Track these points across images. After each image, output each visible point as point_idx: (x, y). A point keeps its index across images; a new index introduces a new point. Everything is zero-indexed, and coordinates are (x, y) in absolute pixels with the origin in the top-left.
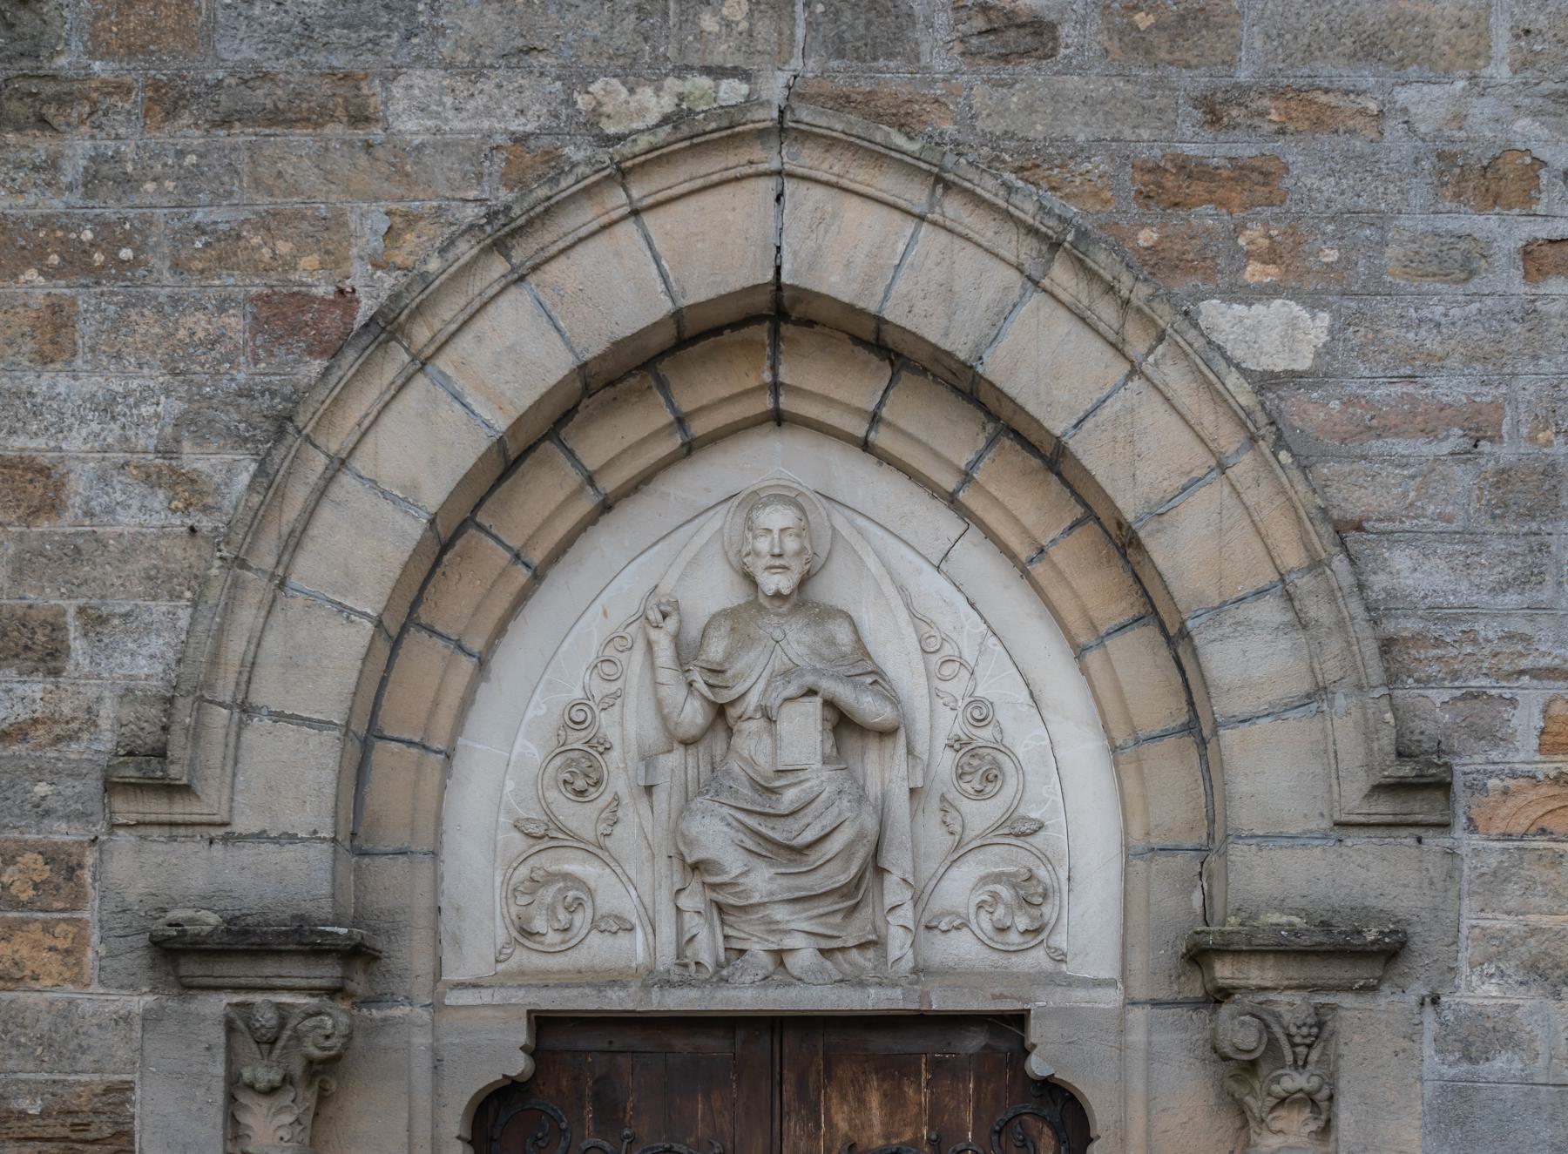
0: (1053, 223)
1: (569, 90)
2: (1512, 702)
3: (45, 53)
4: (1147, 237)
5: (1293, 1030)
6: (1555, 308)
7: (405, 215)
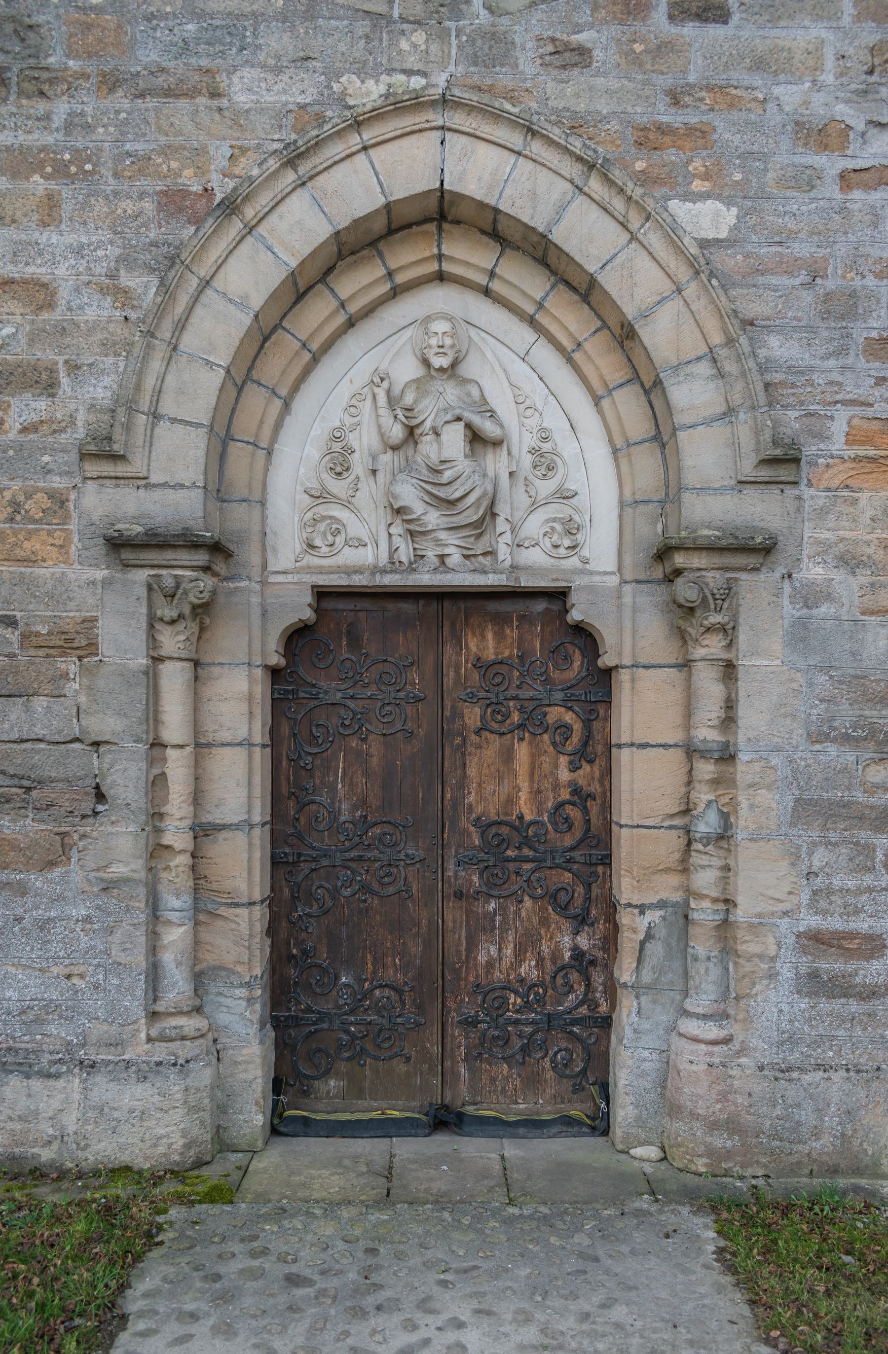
0: (590, 153)
1: (329, 80)
2: (832, 418)
3: (42, 55)
4: (640, 165)
5: (715, 591)
6: (856, 207)
7: (240, 148)
